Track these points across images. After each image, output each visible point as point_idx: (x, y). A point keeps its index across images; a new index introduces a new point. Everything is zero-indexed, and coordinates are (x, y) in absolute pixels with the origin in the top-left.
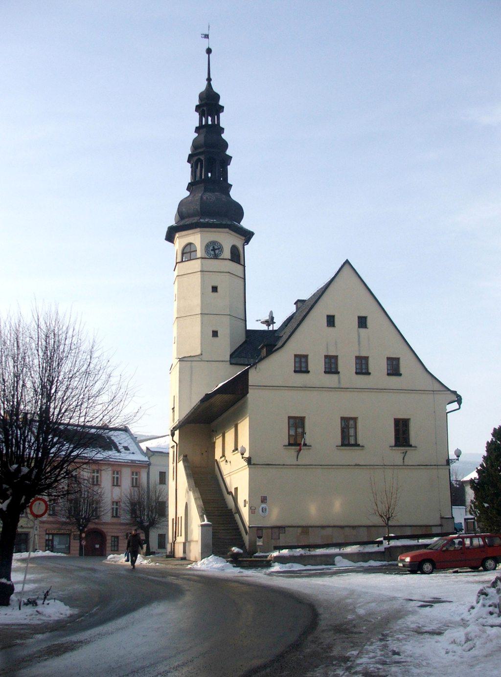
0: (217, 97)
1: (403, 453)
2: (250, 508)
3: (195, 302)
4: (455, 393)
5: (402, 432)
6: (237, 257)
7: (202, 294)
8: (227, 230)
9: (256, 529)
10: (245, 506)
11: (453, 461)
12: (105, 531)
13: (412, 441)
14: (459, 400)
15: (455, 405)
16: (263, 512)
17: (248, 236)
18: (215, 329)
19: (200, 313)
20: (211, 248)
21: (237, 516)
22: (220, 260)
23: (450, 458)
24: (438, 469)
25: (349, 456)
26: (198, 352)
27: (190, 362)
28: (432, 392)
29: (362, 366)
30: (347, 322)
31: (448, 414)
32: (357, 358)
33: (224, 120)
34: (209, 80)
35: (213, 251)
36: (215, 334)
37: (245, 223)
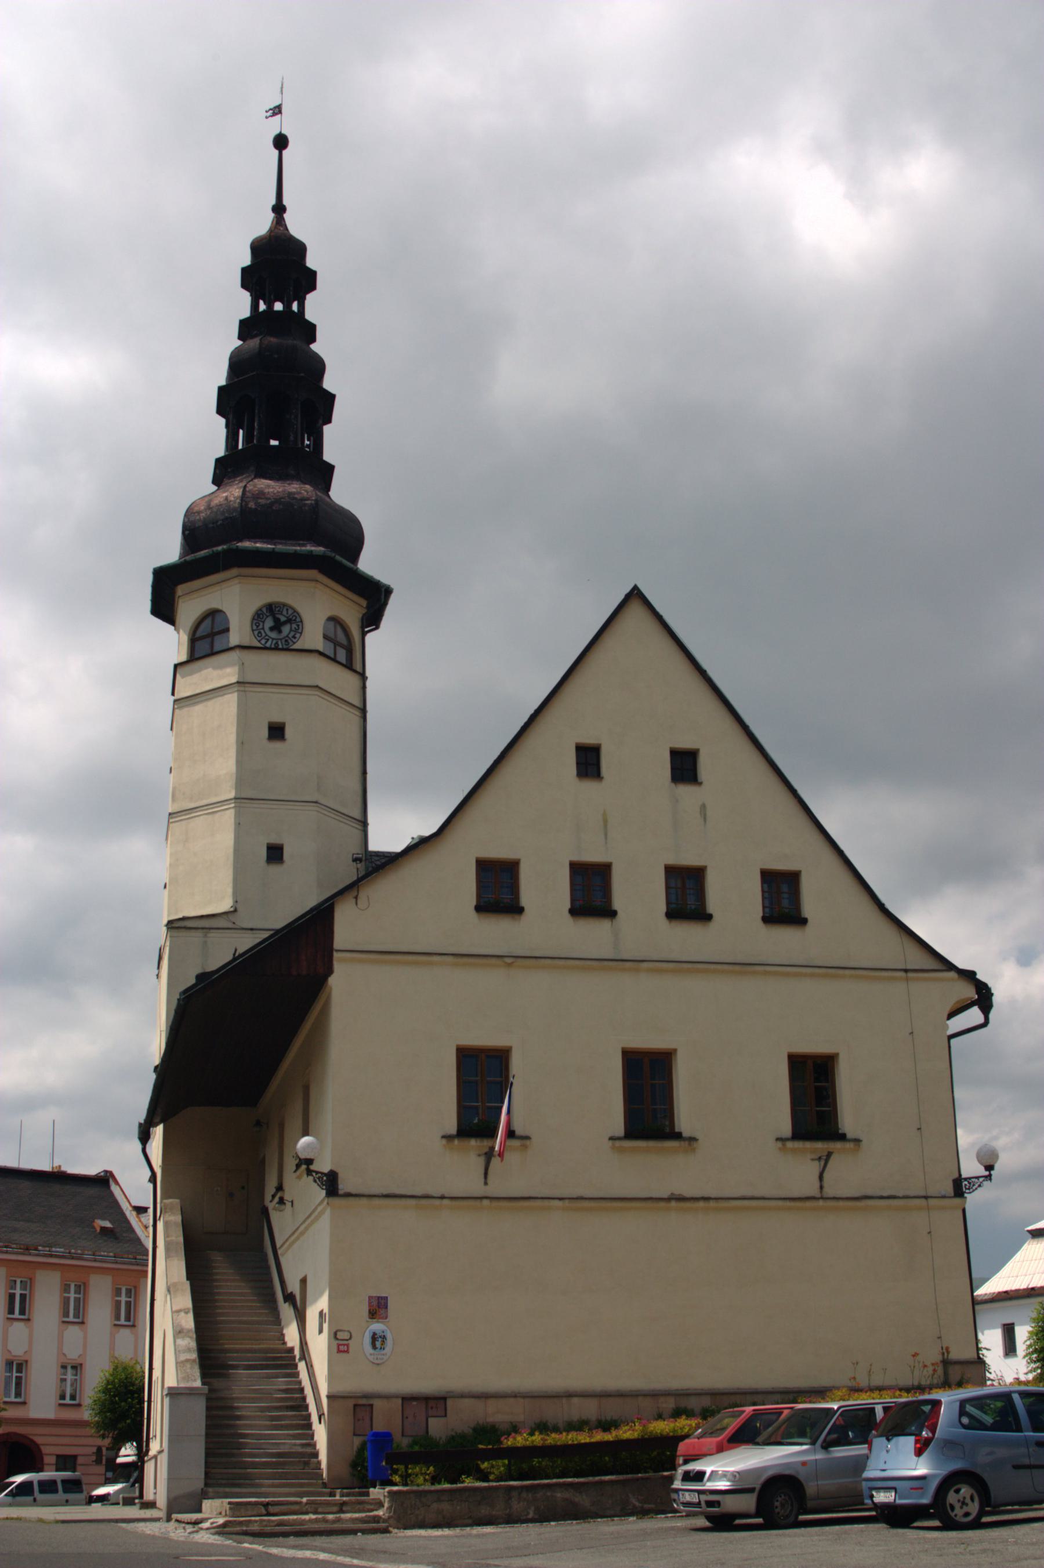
0: (299, 249)
1: (820, 1158)
2: (335, 1335)
3: (222, 767)
4: (969, 975)
5: (814, 1091)
6: (347, 654)
7: (242, 744)
8: (313, 573)
9: (350, 1403)
10: (321, 1331)
11: (974, 1183)
12: (39, 1440)
13: (847, 1122)
14: (984, 997)
15: (974, 1015)
16: (374, 1347)
17: (374, 599)
18: (274, 840)
19: (232, 795)
20: (269, 623)
21: (302, 1366)
22: (294, 653)
23: (964, 1175)
24: (928, 1208)
25: (654, 1169)
26: (225, 905)
27: (199, 934)
28: (902, 974)
29: (686, 895)
30: (637, 768)
31: (953, 1041)
32: (671, 871)
33: (315, 307)
34: (279, 209)
35: (277, 626)
36: (275, 853)
37: (368, 564)
